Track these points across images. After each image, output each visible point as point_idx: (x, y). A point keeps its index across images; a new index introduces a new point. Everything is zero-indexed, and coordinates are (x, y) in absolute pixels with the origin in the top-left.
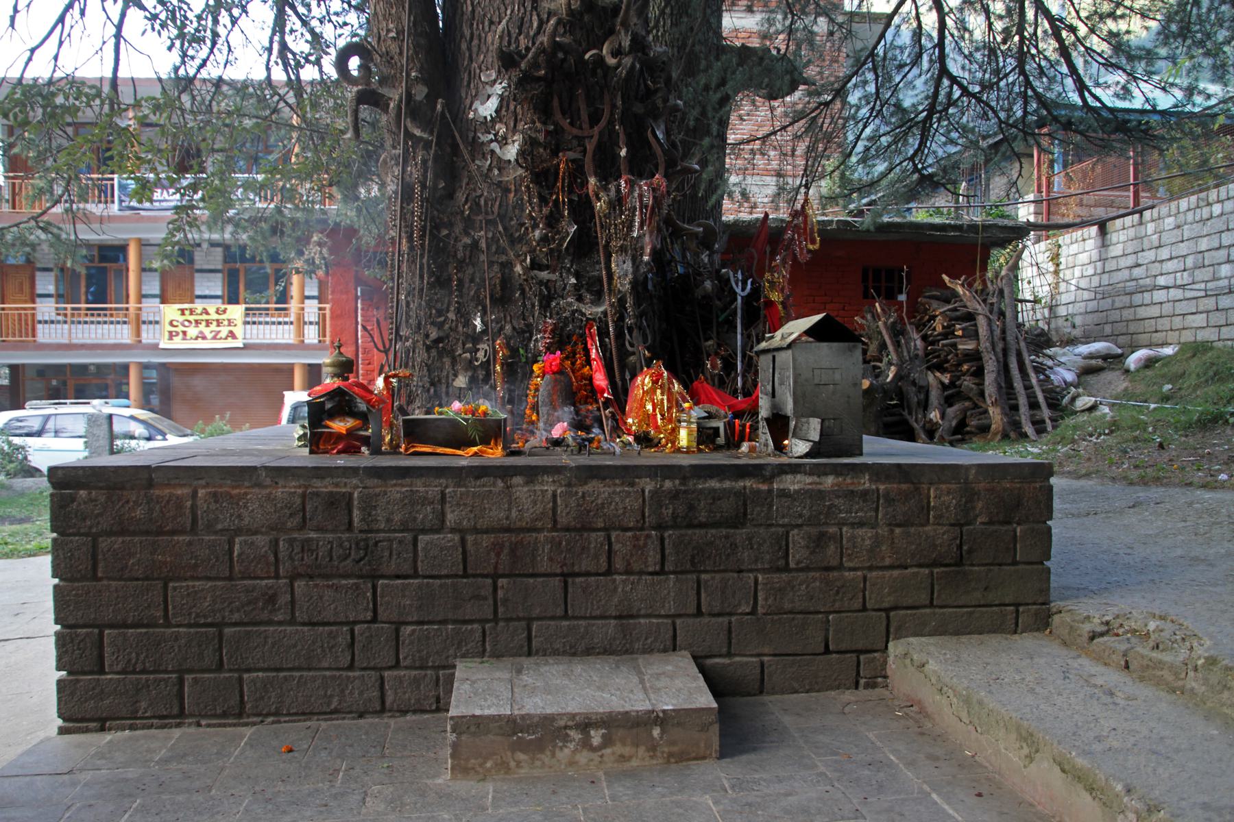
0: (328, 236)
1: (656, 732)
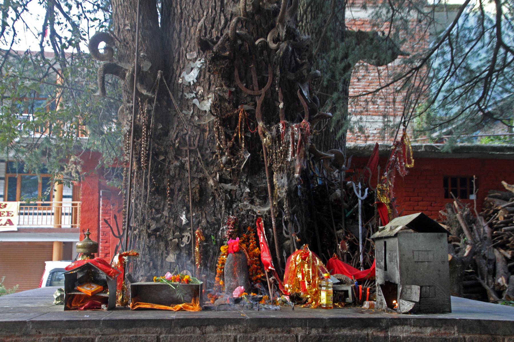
0: (81, 158)
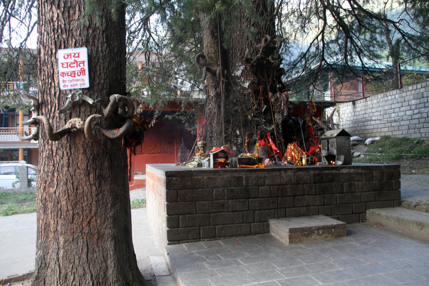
1: (333, 230)
